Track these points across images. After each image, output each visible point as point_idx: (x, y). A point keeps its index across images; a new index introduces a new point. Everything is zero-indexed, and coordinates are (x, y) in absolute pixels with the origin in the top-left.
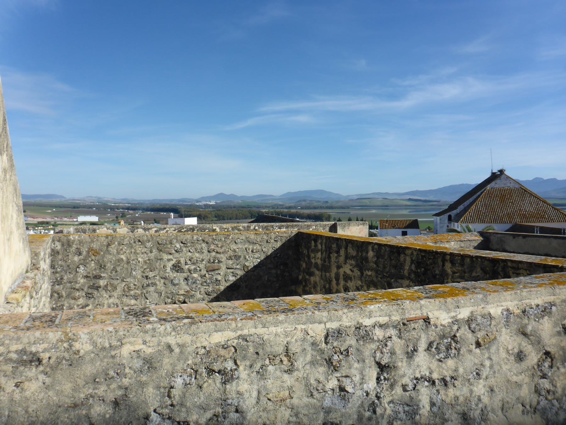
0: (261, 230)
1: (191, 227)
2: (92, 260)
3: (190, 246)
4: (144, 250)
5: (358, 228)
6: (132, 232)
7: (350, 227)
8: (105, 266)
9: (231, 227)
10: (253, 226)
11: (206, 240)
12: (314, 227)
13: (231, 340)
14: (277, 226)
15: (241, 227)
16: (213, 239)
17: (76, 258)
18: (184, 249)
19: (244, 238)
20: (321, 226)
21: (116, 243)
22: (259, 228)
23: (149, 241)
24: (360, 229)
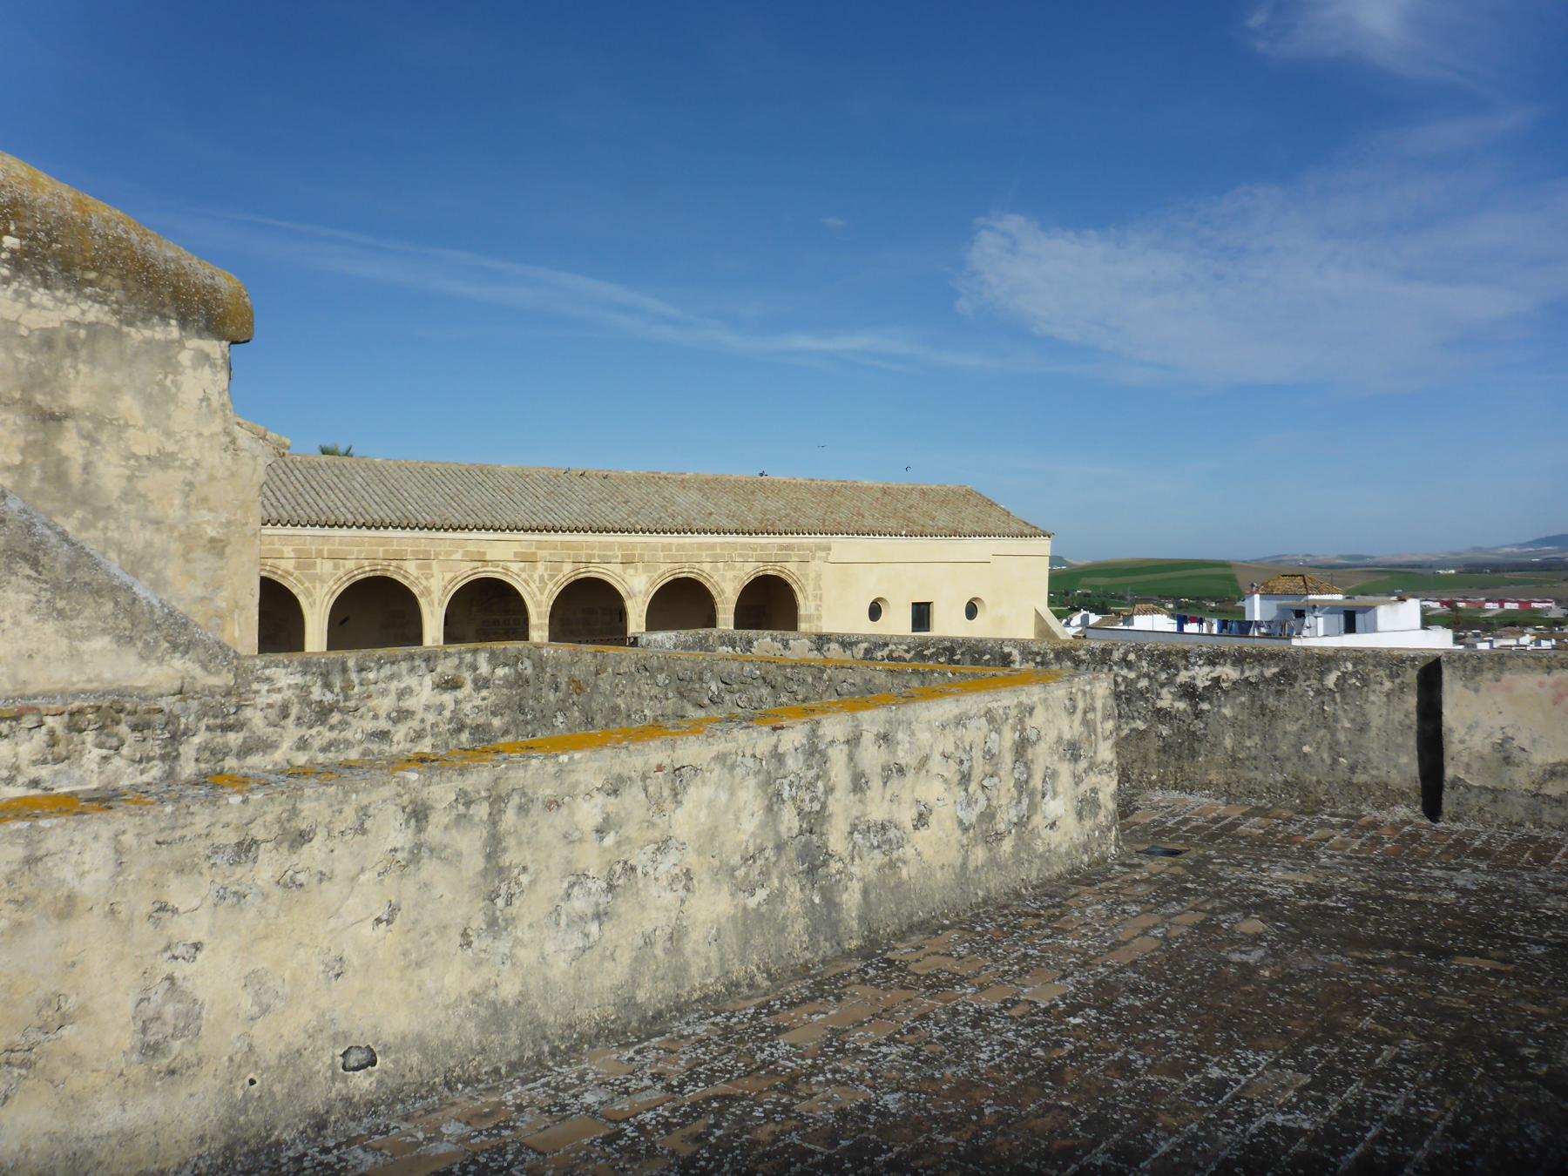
0: (1144, 664)
1: (947, 644)
2: (574, 704)
3: (739, 691)
4: (655, 691)
5: (1549, 679)
6: (819, 649)
7: (1507, 676)
8: (593, 719)
9: (1053, 650)
10: (1121, 650)
11: (770, 677)
12: (1350, 666)
13: (55, 854)
14: (1200, 656)
15: (1081, 652)
16: (786, 677)
17: (552, 697)
18: (727, 697)
19: (858, 680)
20: (1379, 664)
21: (610, 670)
22: (1139, 658)
23: (661, 670)
24: (1556, 685)
